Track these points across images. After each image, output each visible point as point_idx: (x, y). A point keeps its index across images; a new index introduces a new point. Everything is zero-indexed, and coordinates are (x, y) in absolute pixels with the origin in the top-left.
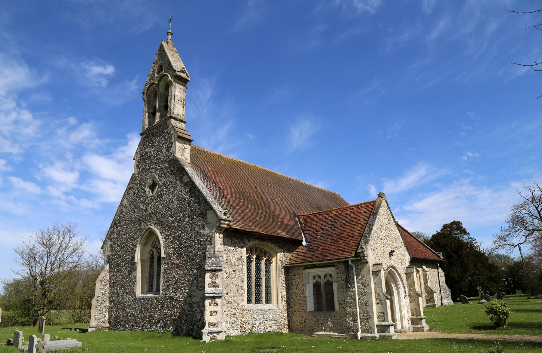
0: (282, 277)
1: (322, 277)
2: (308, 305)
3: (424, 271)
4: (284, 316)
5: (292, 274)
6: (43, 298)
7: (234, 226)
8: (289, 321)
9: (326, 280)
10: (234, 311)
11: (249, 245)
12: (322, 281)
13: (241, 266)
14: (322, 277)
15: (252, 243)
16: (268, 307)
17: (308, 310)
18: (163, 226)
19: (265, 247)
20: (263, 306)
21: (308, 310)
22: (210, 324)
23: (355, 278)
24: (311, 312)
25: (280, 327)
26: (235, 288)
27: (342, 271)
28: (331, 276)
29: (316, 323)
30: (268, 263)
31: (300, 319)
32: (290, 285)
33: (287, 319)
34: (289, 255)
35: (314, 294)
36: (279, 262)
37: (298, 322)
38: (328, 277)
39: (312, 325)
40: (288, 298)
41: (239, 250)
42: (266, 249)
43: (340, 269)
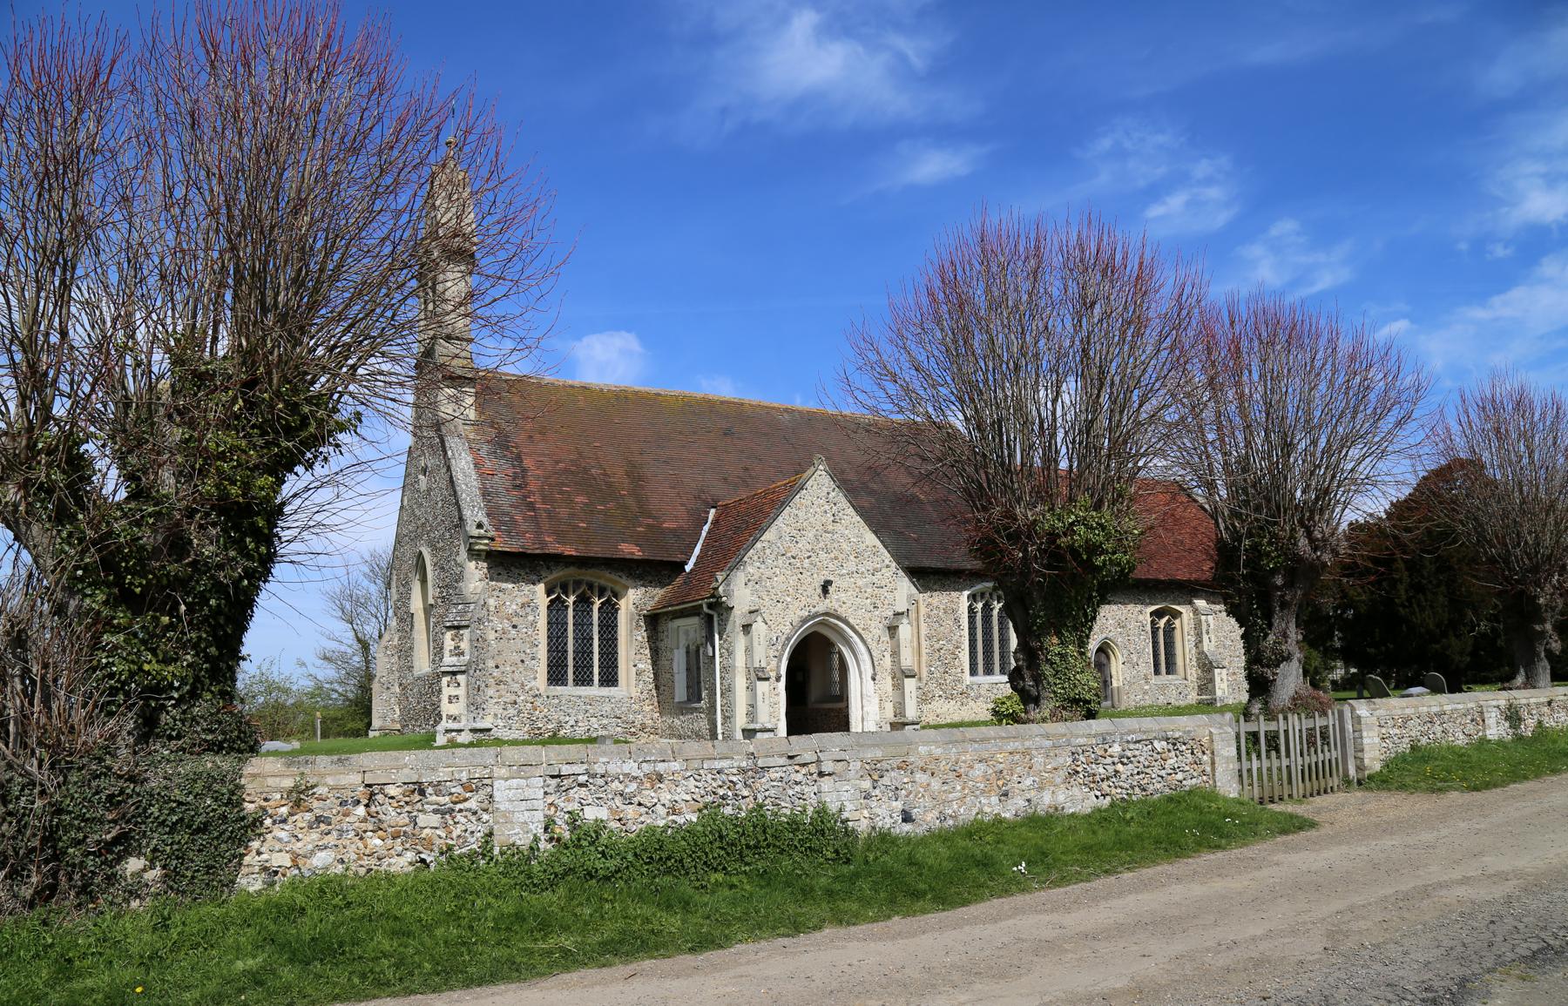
0: (641, 635)
3: (1196, 611)
6: (1559, 677)
7: (499, 546)
10: (514, 697)
11: (551, 577)
13: (531, 618)
15: (558, 574)
16: (606, 691)
18: (434, 548)
20: (595, 690)
22: (449, 717)
26: (516, 658)
30: (610, 611)
34: (658, 593)
36: (631, 607)
41: (527, 588)
42: (603, 582)
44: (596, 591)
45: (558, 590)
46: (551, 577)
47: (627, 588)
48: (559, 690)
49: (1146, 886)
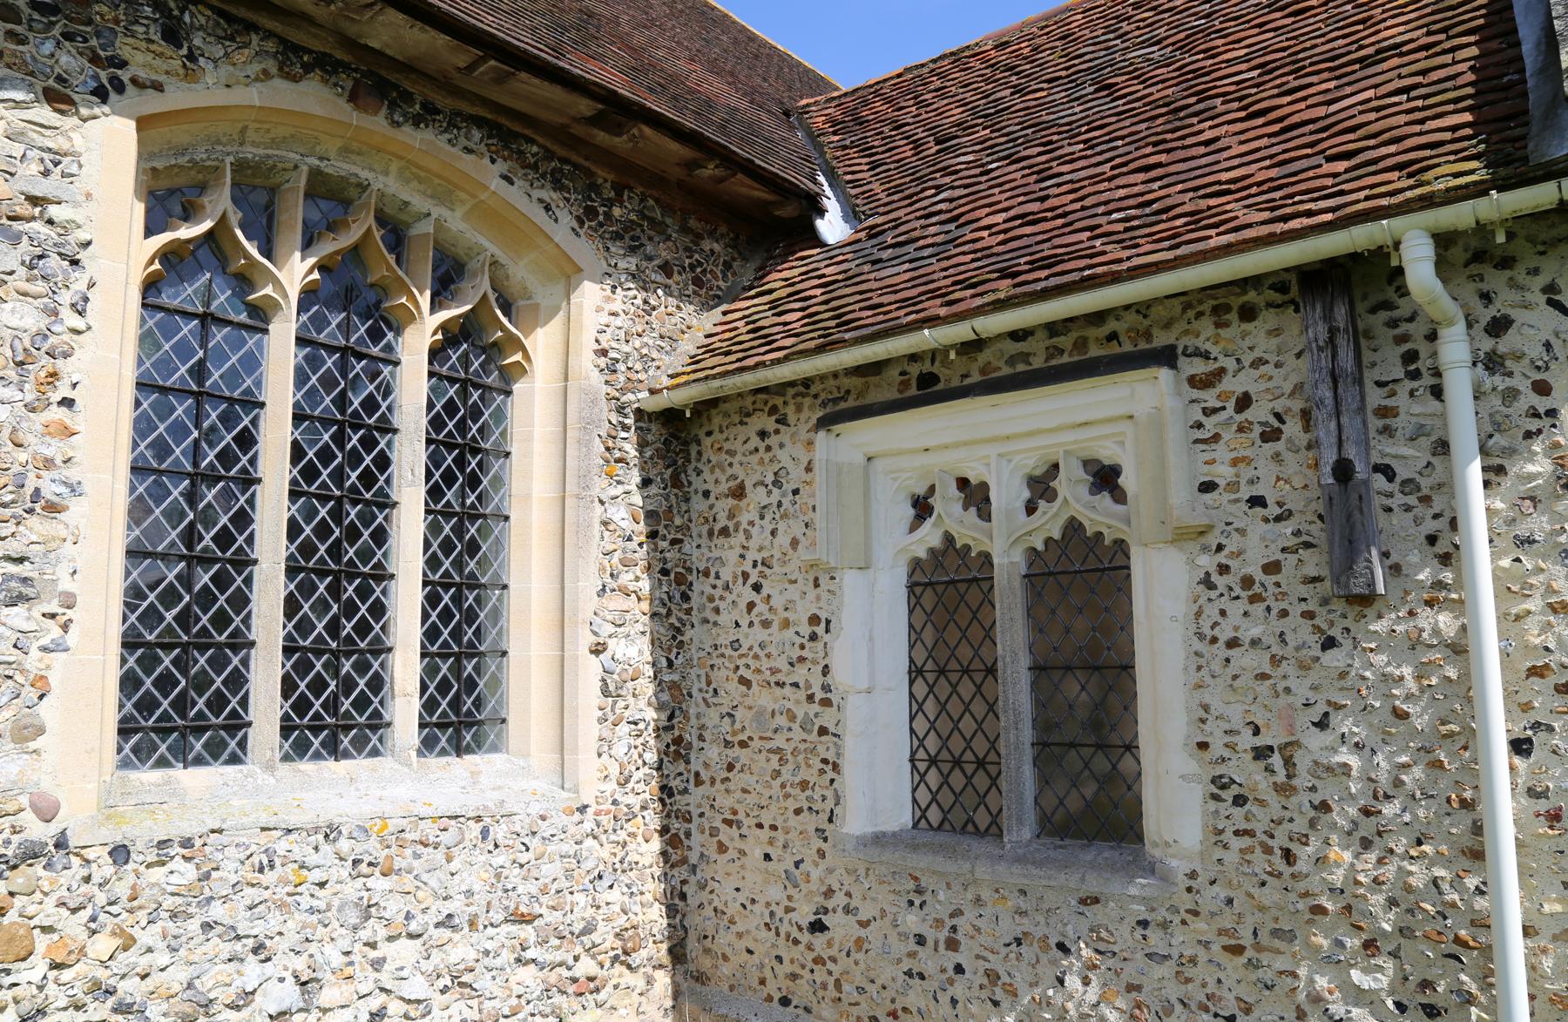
0: (623, 503)
1: (1007, 494)
2: (853, 780)
4: (625, 866)
5: (711, 478)
8: (675, 902)
9: (1049, 521)
12: (1007, 542)
14: (1007, 494)
16: (455, 781)
17: (855, 822)
19: (445, 196)
20: (396, 781)
21: (855, 822)
23: (1474, 473)
24: (879, 840)
25: (586, 967)
27: (1259, 412)
28: (1105, 478)
29: (928, 961)
30: (476, 366)
31: (776, 893)
32: (700, 586)
33: (654, 888)
35: (915, 672)
36: (586, 364)
37: (752, 922)
38: (1076, 498)
39: (889, 973)
40: (674, 702)
42: (458, 224)
43: (1234, 384)
44: (294, 213)
45: (220, 202)
46: (178, 97)
47: (570, 275)
48: (196, 792)
49: (529, 439)
